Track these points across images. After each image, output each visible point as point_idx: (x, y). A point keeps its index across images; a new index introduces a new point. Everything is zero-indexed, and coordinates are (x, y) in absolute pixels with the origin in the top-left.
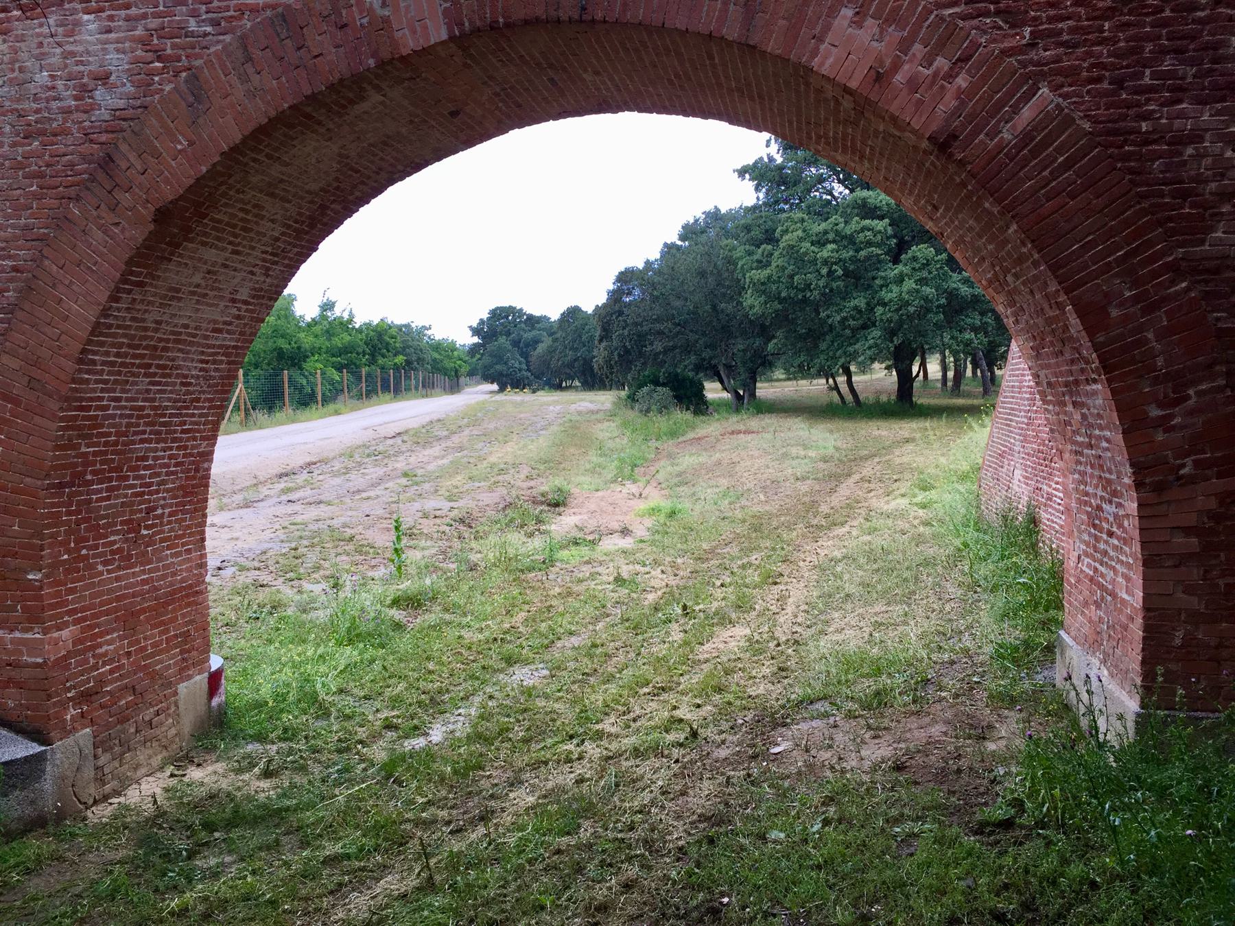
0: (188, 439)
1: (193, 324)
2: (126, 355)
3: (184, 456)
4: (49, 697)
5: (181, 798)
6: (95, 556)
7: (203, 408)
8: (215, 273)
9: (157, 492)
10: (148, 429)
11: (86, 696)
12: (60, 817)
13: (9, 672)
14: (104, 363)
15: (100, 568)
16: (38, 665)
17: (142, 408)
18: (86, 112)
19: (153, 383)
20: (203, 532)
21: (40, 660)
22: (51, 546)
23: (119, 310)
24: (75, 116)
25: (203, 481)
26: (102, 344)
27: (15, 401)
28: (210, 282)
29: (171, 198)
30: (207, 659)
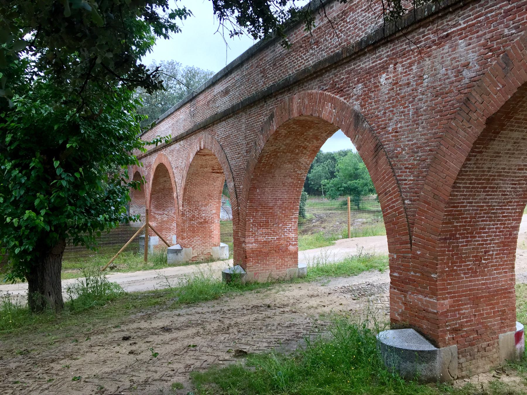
0: (506, 220)
1: (507, 167)
2: (474, 183)
3: (504, 228)
4: (439, 328)
5: (495, 389)
6: (460, 270)
7: (514, 206)
8: (518, 143)
9: (490, 244)
10: (485, 216)
11: (455, 331)
12: (442, 380)
13: (424, 313)
14: (464, 187)
15: (462, 275)
16: (434, 313)
17: (483, 206)
18: (459, 81)
19: (488, 195)
20: (513, 264)
21: (435, 311)
22: (441, 264)
23: (470, 164)
24: (455, 84)
25: (514, 240)
26: (463, 179)
27: (429, 204)
28: (516, 147)
29: (494, 112)
30: (515, 325)
